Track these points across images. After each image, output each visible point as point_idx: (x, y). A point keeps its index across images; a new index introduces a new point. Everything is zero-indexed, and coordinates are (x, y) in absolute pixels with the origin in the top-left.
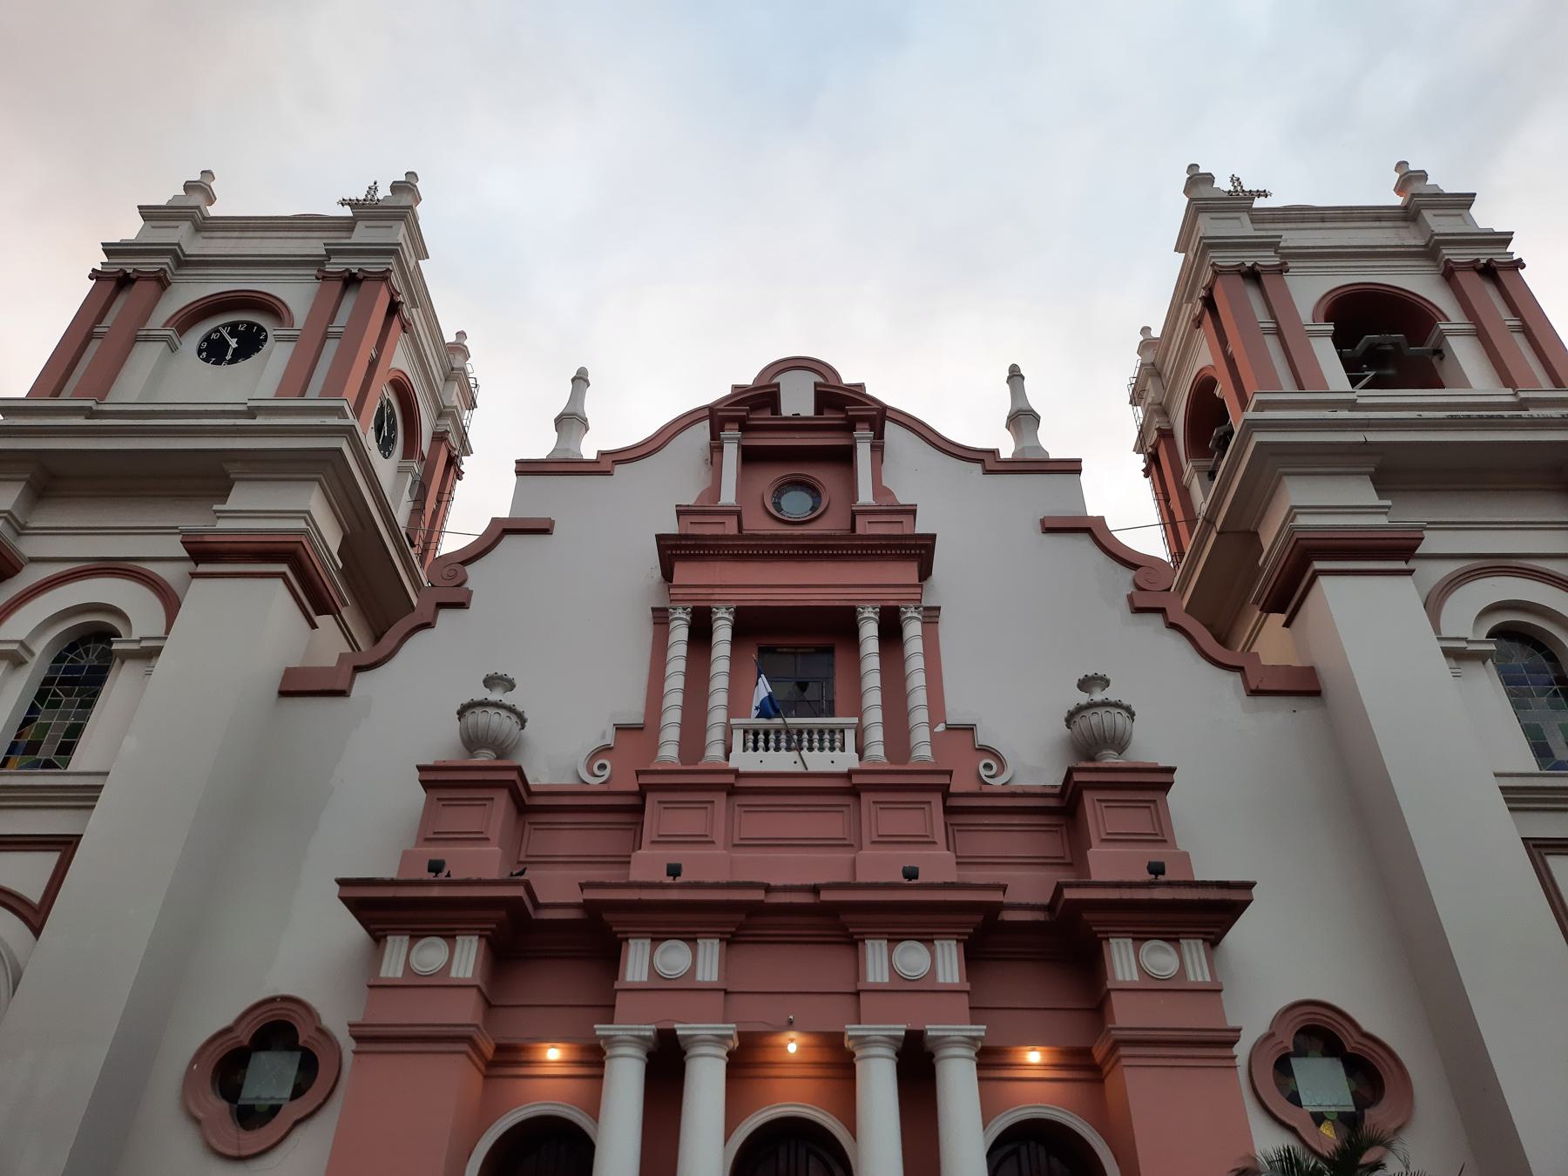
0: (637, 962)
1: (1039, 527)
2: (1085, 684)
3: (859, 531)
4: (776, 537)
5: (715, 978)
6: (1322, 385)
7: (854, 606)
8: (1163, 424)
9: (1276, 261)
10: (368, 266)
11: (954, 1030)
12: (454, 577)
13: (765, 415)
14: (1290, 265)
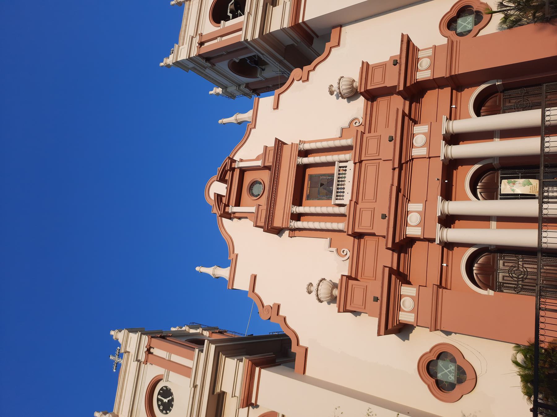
0: (413, 231)
1: (276, 111)
2: (332, 93)
3: (263, 225)
4: (268, 198)
5: (415, 289)
6: (242, 23)
7: (291, 214)
8: (244, 86)
9: (198, 37)
10: (145, 344)
11: (444, 125)
12: (268, 310)
13: (224, 200)
14: (200, 33)
